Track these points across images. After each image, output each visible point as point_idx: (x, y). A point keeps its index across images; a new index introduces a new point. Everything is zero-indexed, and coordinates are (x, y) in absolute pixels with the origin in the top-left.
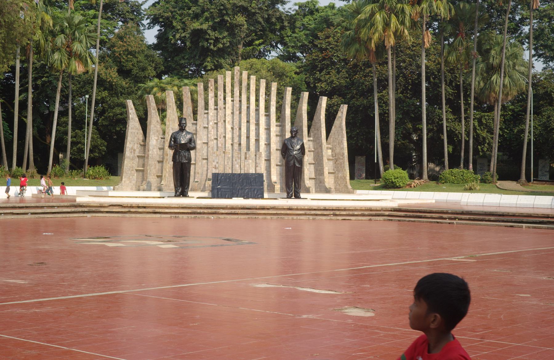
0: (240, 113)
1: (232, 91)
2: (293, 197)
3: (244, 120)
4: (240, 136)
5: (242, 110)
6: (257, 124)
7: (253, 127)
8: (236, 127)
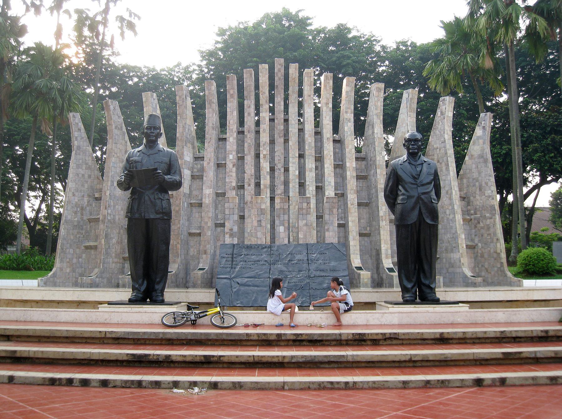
0: (286, 141)
1: (272, 99)
2: (418, 300)
3: (294, 153)
4: (286, 183)
5: (291, 134)
6: (319, 159)
7: (310, 164)
8: (279, 166)
